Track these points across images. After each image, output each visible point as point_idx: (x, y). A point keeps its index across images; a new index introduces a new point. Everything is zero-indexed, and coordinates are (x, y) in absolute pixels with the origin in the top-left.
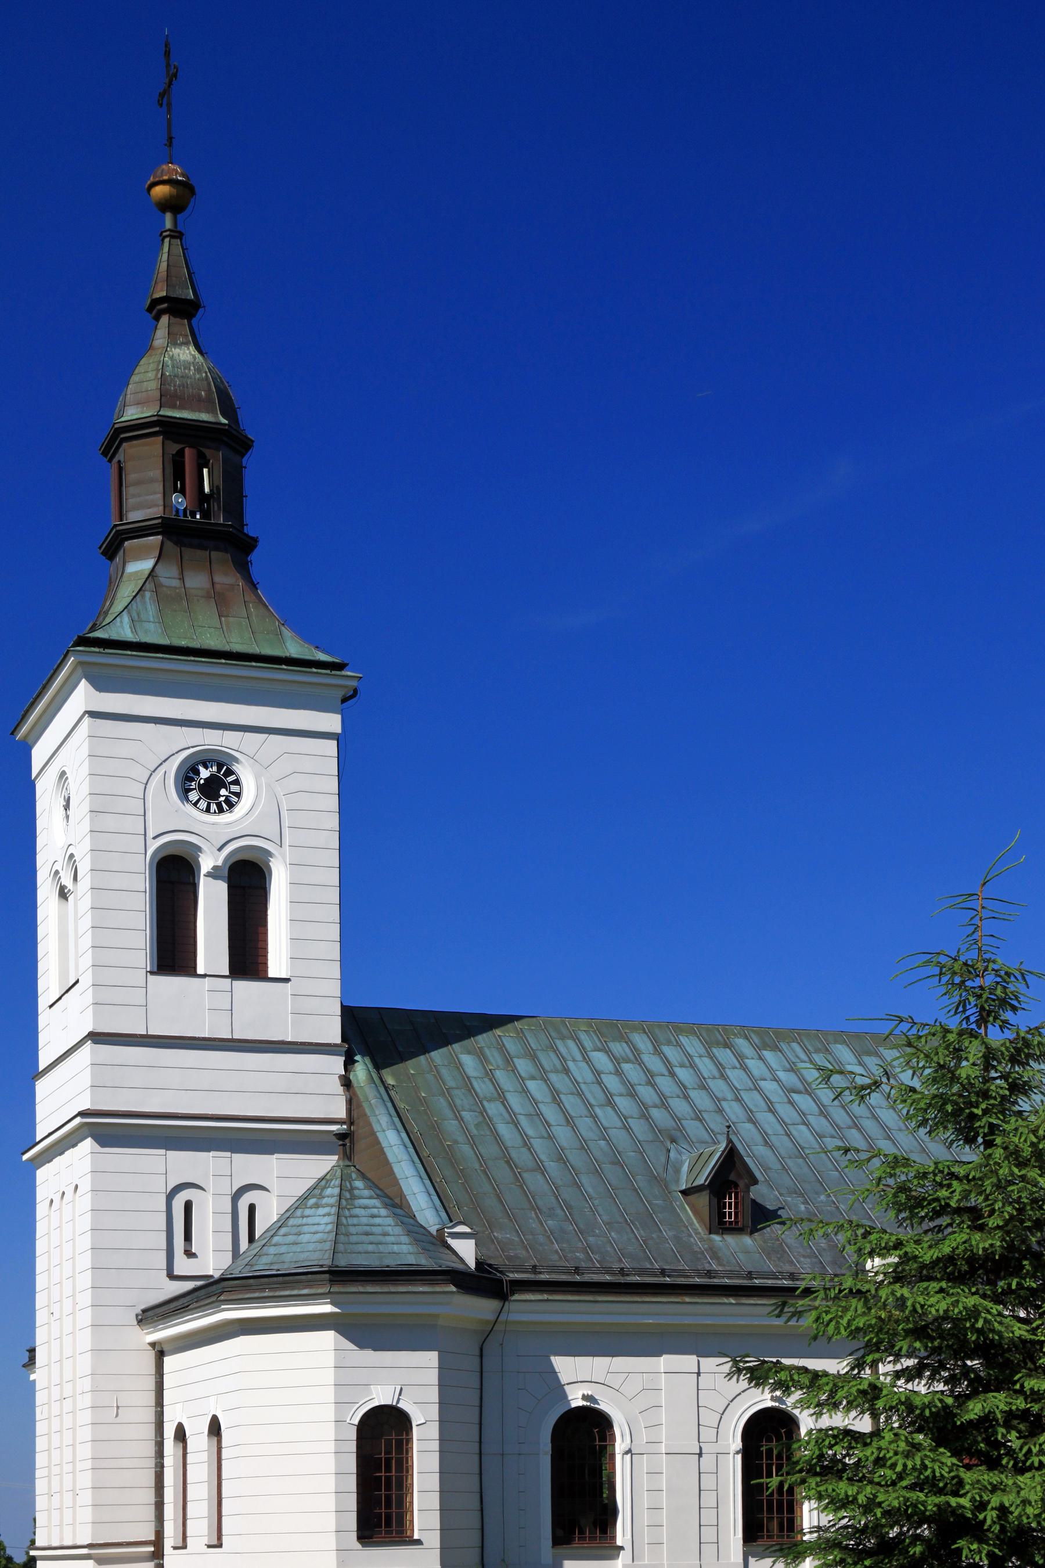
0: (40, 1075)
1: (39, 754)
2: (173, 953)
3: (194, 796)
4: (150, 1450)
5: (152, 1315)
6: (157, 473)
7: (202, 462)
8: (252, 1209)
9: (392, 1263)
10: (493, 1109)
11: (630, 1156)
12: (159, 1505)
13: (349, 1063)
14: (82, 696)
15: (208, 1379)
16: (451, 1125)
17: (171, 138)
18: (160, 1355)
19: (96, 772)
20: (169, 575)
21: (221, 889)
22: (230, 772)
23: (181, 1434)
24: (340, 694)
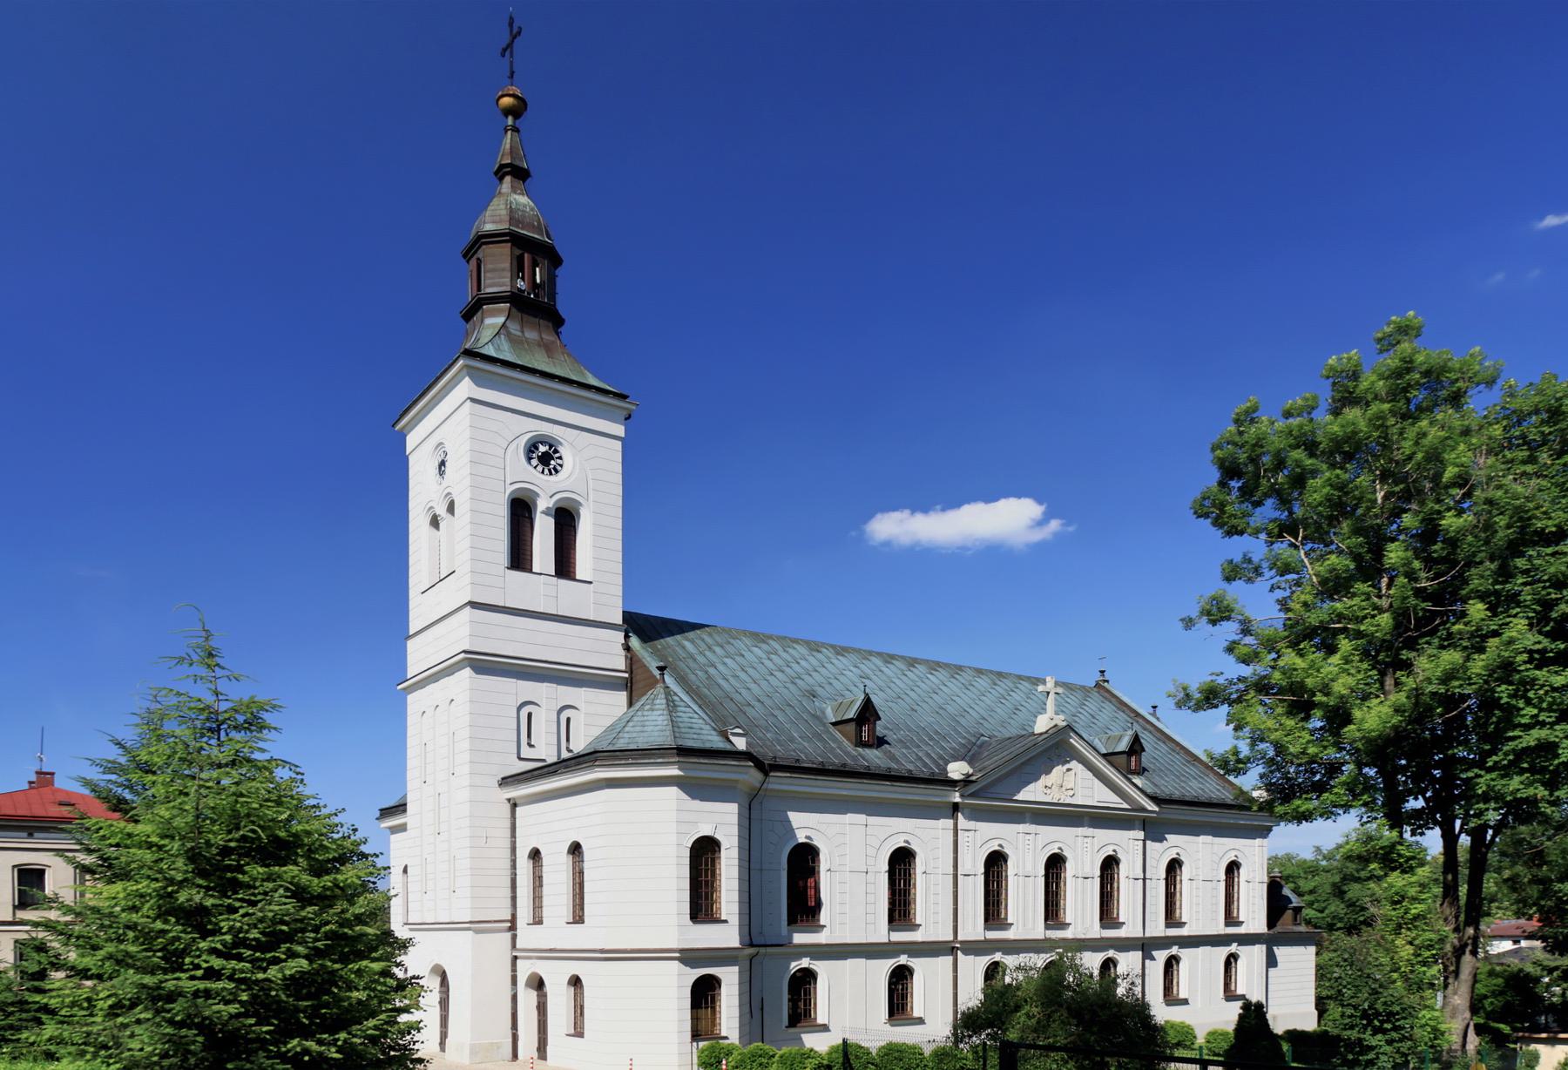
0: (409, 637)
1: (412, 440)
2: (519, 558)
3: (535, 462)
4: (508, 864)
5: (506, 781)
6: (507, 265)
7: (535, 264)
8: (568, 720)
9: (708, 746)
10: (711, 671)
11: (794, 703)
12: (514, 898)
13: (627, 637)
14: (466, 387)
15: (550, 823)
16: (692, 677)
17: (512, 73)
18: (515, 805)
19: (462, 445)
20: (514, 328)
21: (551, 522)
22: (556, 451)
23: (535, 855)
24: (625, 413)
